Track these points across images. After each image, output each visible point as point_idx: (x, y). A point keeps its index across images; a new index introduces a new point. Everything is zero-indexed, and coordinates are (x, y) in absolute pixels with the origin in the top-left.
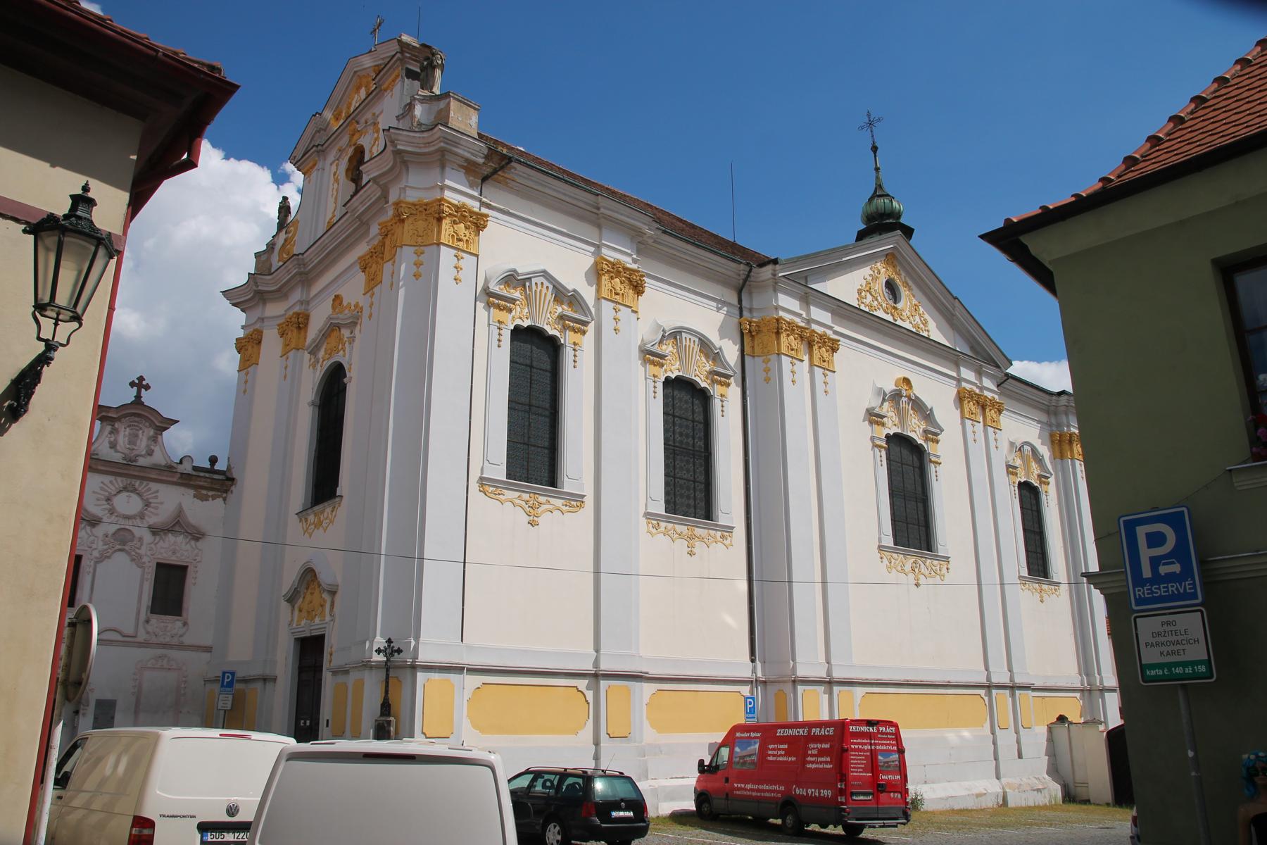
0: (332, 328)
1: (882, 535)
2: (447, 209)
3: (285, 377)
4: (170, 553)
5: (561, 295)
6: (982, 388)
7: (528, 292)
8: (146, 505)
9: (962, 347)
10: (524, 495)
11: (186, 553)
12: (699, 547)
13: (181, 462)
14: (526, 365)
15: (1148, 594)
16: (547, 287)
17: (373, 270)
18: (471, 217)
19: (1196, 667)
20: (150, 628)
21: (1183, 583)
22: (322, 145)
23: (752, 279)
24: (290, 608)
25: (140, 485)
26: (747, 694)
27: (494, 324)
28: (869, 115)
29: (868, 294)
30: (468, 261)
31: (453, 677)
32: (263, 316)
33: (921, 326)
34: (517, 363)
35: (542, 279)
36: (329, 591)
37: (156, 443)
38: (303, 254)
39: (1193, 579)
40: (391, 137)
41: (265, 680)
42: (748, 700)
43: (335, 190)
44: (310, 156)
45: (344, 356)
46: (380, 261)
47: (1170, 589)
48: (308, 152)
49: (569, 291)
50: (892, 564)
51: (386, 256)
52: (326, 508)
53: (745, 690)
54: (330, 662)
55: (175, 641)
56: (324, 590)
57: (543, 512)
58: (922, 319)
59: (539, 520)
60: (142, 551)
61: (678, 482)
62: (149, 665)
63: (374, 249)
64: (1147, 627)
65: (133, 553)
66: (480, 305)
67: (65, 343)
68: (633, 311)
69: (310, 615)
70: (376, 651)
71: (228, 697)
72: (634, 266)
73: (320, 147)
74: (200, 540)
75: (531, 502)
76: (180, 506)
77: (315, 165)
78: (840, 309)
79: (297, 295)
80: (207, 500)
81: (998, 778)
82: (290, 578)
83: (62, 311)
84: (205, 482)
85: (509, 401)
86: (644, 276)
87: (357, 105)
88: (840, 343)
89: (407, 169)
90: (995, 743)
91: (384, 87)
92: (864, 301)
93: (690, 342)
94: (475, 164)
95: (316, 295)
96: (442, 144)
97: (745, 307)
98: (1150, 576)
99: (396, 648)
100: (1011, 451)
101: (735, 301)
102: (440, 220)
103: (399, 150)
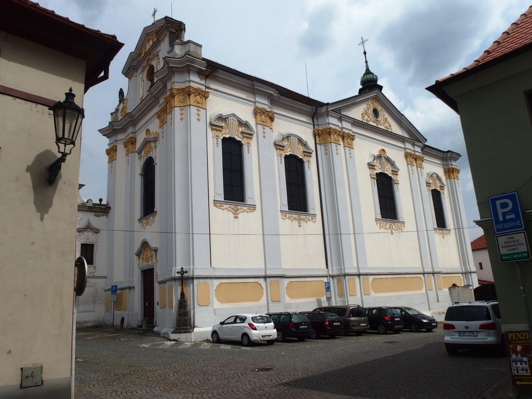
0: (147, 142)
1: (377, 214)
2: (192, 90)
3: (128, 164)
4: (86, 239)
5: (242, 123)
6: (415, 151)
9: (406, 135)
10: (231, 206)
11: (93, 239)
13: (88, 202)
14: (229, 153)
15: (502, 227)
17: (162, 118)
18: (202, 93)
19: (523, 254)
21: (516, 222)
22: (135, 66)
23: (318, 112)
24: (138, 259)
26: (326, 281)
27: (215, 137)
28: (362, 39)
29: (366, 116)
30: (202, 112)
31: (209, 281)
32: (116, 140)
33: (389, 127)
35: (233, 118)
36: (154, 250)
38: (131, 113)
39: (520, 220)
40: (166, 61)
42: (326, 284)
43: (142, 85)
44: (131, 70)
46: (165, 114)
47: (511, 224)
48: (129, 69)
49: (244, 122)
50: (381, 226)
51: (168, 112)
53: (325, 280)
54: (157, 279)
56: (152, 250)
58: (389, 124)
59: (239, 216)
63: (162, 109)
64: (502, 240)
66: (209, 130)
67: (69, 153)
68: (270, 128)
70: (177, 273)
71: (115, 296)
72: (270, 110)
73: (134, 67)
74: (98, 234)
75: (235, 209)
76: (89, 219)
77: (133, 75)
78: (356, 123)
79: (130, 130)
80: (100, 217)
81: (430, 310)
82: (137, 246)
83: (67, 140)
84: (98, 209)
86: (274, 114)
87: (149, 48)
88: (355, 136)
89: (174, 75)
90: (427, 296)
91: (160, 39)
92: (364, 118)
95: (138, 130)
96: (188, 63)
98: (502, 220)
99: (185, 271)
100: (427, 176)
102: (189, 95)
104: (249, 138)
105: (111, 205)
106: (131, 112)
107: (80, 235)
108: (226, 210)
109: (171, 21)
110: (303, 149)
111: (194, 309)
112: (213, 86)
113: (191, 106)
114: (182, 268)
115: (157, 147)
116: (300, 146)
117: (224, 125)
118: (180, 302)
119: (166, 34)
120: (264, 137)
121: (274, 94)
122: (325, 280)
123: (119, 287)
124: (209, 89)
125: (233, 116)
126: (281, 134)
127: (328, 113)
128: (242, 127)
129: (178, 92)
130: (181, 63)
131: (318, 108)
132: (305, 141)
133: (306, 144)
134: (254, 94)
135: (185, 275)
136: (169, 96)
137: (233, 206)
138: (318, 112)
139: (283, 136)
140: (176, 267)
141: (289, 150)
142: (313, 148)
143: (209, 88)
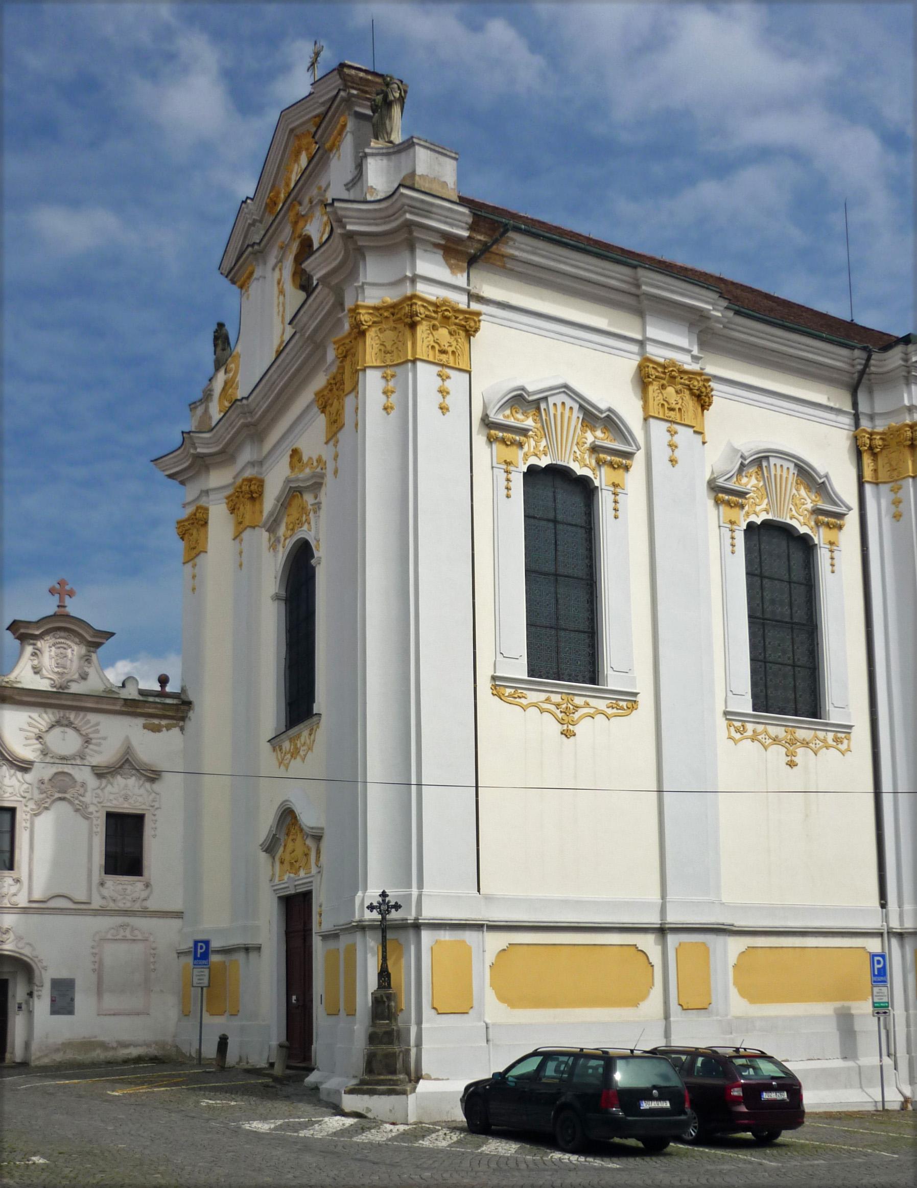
2: (422, 310)
3: (241, 565)
4: (121, 800)
7: (544, 417)
8: (87, 742)
11: (140, 799)
12: (802, 754)
13: (124, 685)
14: (548, 520)
16: (571, 408)
17: (333, 410)
18: (456, 318)
20: (105, 892)
23: (873, 369)
24: (270, 860)
25: (76, 717)
30: (457, 381)
31: (470, 937)
34: (534, 518)
37: (89, 663)
38: (247, 398)
40: (335, 213)
41: (247, 949)
42: (876, 958)
45: (310, 530)
49: (601, 412)
51: (348, 386)
52: (303, 730)
53: (874, 945)
55: (137, 907)
57: (581, 718)
60: (87, 799)
61: (771, 668)
62: (109, 937)
63: (334, 379)
65: (77, 802)
66: (480, 440)
68: (696, 432)
69: (294, 866)
70: (368, 908)
72: (695, 367)
73: (256, 247)
74: (157, 781)
75: (564, 706)
76: (127, 739)
77: (252, 273)
79: (247, 455)
80: (159, 731)
84: (156, 708)
85: (526, 571)
86: (709, 380)
89: (364, 258)
91: (328, 145)
93: (782, 471)
94: (458, 240)
96: (408, 216)
97: (863, 413)
99: (392, 903)
101: (848, 408)
102: (413, 326)
103: (350, 231)
104: (619, 467)
105: (191, 696)
106: (246, 395)
107: (103, 785)
108: (533, 711)
109: (361, 78)
110: (813, 501)
111: (419, 1023)
112: (489, 290)
113: (419, 364)
114: (384, 895)
115: (323, 506)
116: (803, 492)
117: (533, 424)
118: (375, 997)
119: (344, 126)
120: (673, 461)
121: (710, 310)
122: (874, 945)
123: (215, 944)
124: (483, 304)
125: (564, 392)
126: (736, 451)
127: (909, 372)
128: (593, 429)
129: (375, 319)
130: (387, 219)
131: (873, 357)
132: (822, 473)
133: (823, 483)
134: (640, 313)
135: (394, 915)
136: (350, 334)
137: (559, 696)
138: (873, 369)
139: (742, 457)
140: (365, 889)
141: (764, 506)
142: (852, 499)
143: (480, 299)
